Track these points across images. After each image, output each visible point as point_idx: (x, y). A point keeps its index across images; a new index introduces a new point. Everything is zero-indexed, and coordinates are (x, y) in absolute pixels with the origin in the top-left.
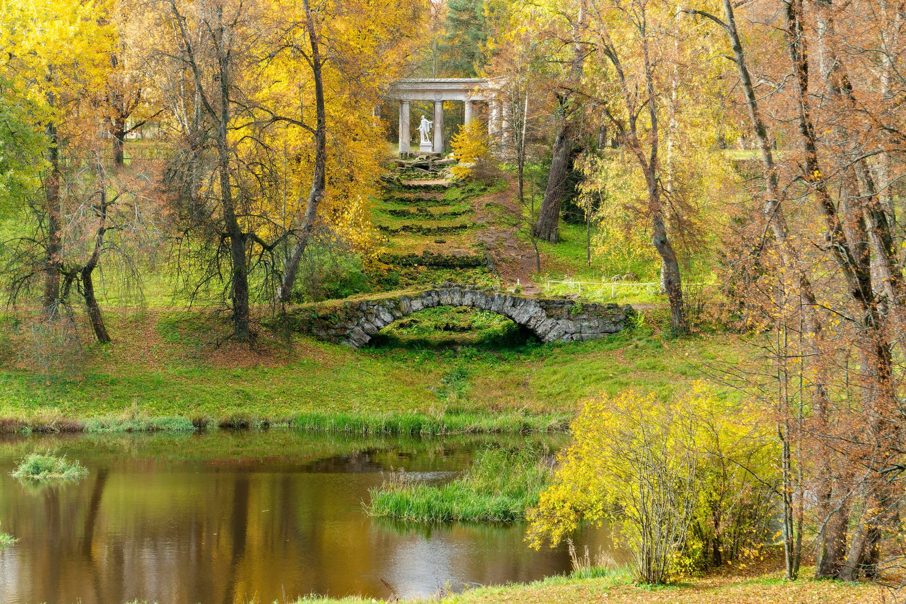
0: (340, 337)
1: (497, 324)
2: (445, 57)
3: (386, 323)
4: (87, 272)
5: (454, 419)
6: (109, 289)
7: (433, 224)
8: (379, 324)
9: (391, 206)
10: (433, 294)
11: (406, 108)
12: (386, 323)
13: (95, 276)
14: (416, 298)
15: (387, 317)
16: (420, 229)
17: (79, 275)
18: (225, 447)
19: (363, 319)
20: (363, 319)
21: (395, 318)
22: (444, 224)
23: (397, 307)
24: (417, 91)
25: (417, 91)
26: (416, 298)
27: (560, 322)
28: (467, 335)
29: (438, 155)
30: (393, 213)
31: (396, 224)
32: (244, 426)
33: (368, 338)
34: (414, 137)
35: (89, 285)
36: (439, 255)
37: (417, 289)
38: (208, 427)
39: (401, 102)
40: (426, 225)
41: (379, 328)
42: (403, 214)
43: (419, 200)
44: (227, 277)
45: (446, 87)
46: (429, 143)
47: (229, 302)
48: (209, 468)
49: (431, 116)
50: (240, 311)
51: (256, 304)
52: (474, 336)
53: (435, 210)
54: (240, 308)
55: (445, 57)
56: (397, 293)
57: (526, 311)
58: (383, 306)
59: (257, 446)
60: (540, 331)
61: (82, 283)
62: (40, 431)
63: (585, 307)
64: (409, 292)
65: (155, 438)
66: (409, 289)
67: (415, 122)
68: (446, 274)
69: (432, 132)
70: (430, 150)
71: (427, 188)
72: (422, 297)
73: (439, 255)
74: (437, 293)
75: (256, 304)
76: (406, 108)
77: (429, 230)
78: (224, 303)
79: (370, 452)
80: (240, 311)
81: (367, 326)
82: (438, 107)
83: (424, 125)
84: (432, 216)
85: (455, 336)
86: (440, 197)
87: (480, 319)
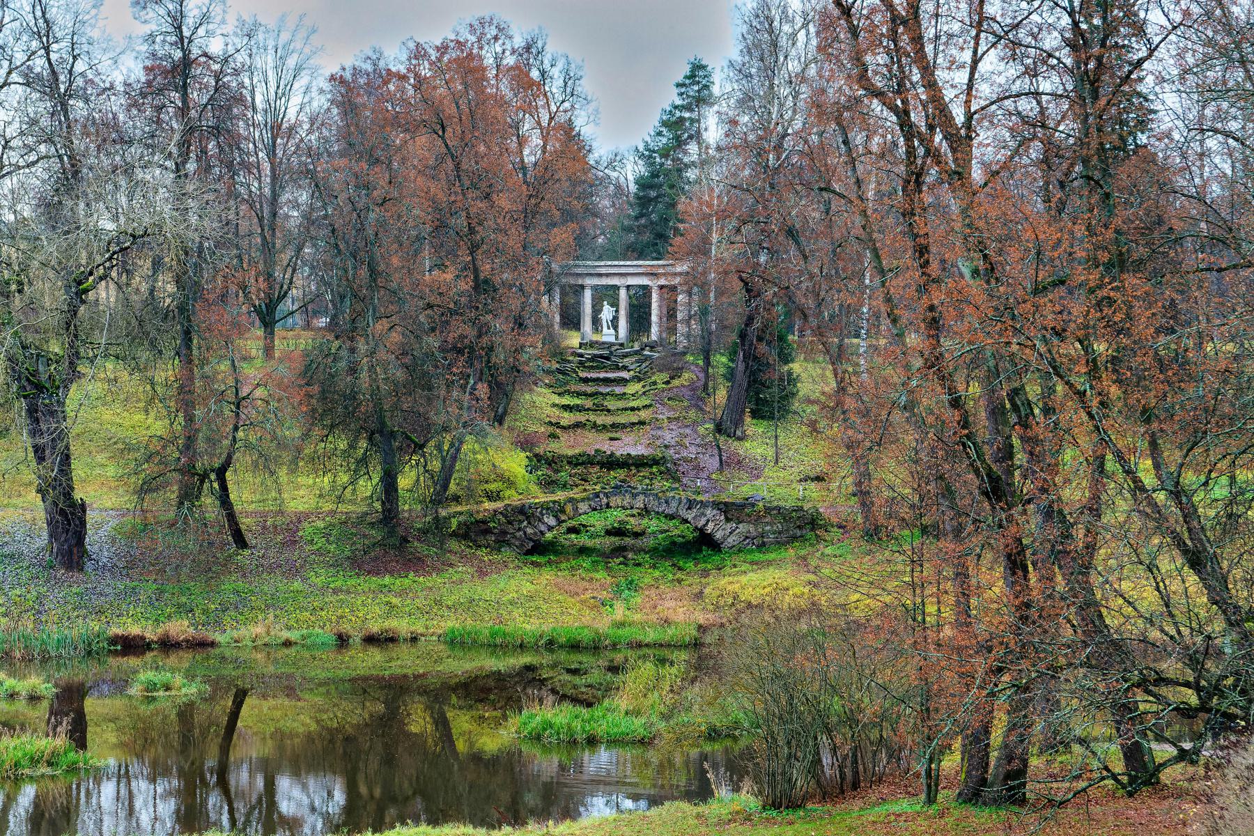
0: (502, 541)
1: (677, 530)
2: (632, 237)
3: (550, 528)
4: (221, 473)
5: (620, 632)
6: (246, 492)
7: (609, 420)
8: (543, 528)
9: (566, 400)
10: (601, 496)
11: (588, 294)
12: (550, 528)
13: (229, 475)
14: (583, 500)
15: (552, 521)
16: (595, 426)
17: (213, 476)
18: (370, 661)
19: (525, 523)
20: (525, 523)
21: (560, 522)
22: (621, 419)
23: (563, 511)
24: (600, 275)
25: (600, 275)
26: (583, 500)
27: (741, 526)
28: (639, 542)
29: (622, 345)
30: (566, 408)
31: (567, 418)
32: (393, 640)
33: (531, 544)
34: (596, 322)
35: (224, 487)
36: (612, 454)
37: (585, 490)
38: (351, 641)
39: (583, 287)
40: (601, 419)
41: (542, 533)
42: (579, 409)
43: (597, 393)
44: (376, 480)
45: (631, 270)
46: (612, 331)
47: (378, 505)
48: (362, 686)
49: (615, 304)
50: (389, 515)
51: (407, 507)
52: (650, 542)
53: (611, 404)
54: (389, 511)
55: (632, 237)
56: (560, 495)
57: (703, 514)
58: (548, 509)
59: (404, 662)
60: (719, 535)
61: (216, 485)
62: (168, 645)
63: (768, 510)
64: (575, 493)
65: (292, 651)
66: (576, 490)
67: (597, 311)
68: (621, 473)
69: (615, 320)
70: (612, 339)
71: (607, 381)
72: (588, 499)
73: (612, 454)
74: (606, 495)
75: (407, 507)
76: (588, 294)
77: (604, 426)
78: (370, 505)
79: (529, 668)
80: (389, 515)
81: (529, 531)
82: (623, 293)
83: (607, 313)
84: (609, 411)
85: (628, 541)
86: (618, 390)
87: (653, 524)
